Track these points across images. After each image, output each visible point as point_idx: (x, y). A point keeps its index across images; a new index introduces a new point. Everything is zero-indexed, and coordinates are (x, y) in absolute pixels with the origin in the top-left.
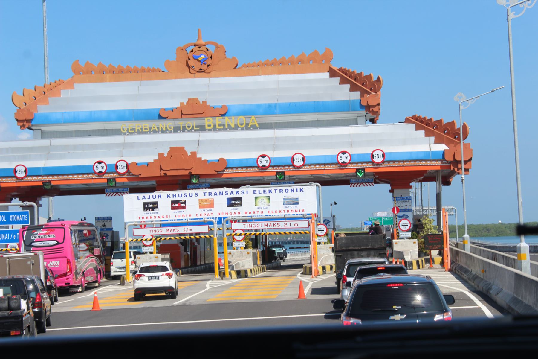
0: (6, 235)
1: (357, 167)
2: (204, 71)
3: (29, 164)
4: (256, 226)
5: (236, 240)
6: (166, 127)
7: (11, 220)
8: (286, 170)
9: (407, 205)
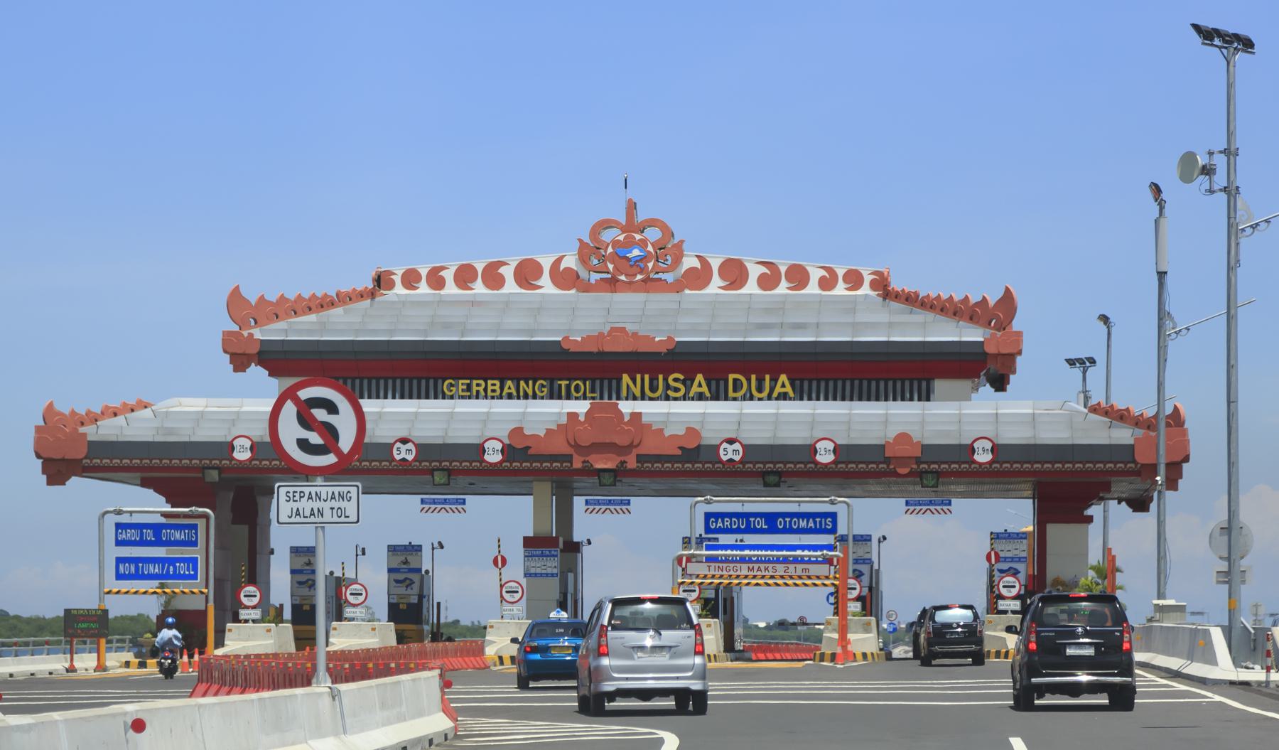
0: (157, 565)
7: (164, 539)
9: (1017, 549)
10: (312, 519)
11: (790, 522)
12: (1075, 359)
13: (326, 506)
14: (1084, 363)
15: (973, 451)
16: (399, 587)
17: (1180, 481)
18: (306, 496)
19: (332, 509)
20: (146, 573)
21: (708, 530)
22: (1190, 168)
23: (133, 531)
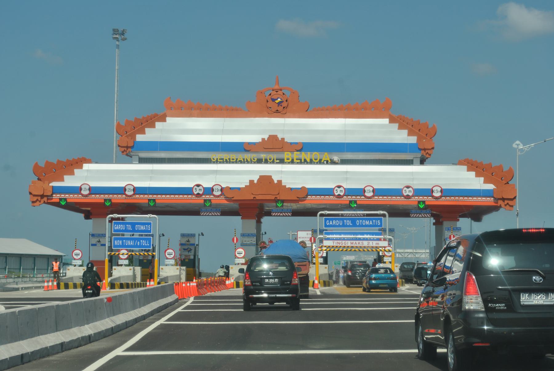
0: (132, 241)
1: (419, 200)
2: (280, 112)
3: (137, 184)
4: (344, 243)
5: (237, 257)
6: (251, 159)
7: (136, 229)
8: (358, 199)
11: (362, 222)
15: (364, 191)
16: (185, 252)
20: (127, 245)
21: (326, 226)
23: (122, 225)
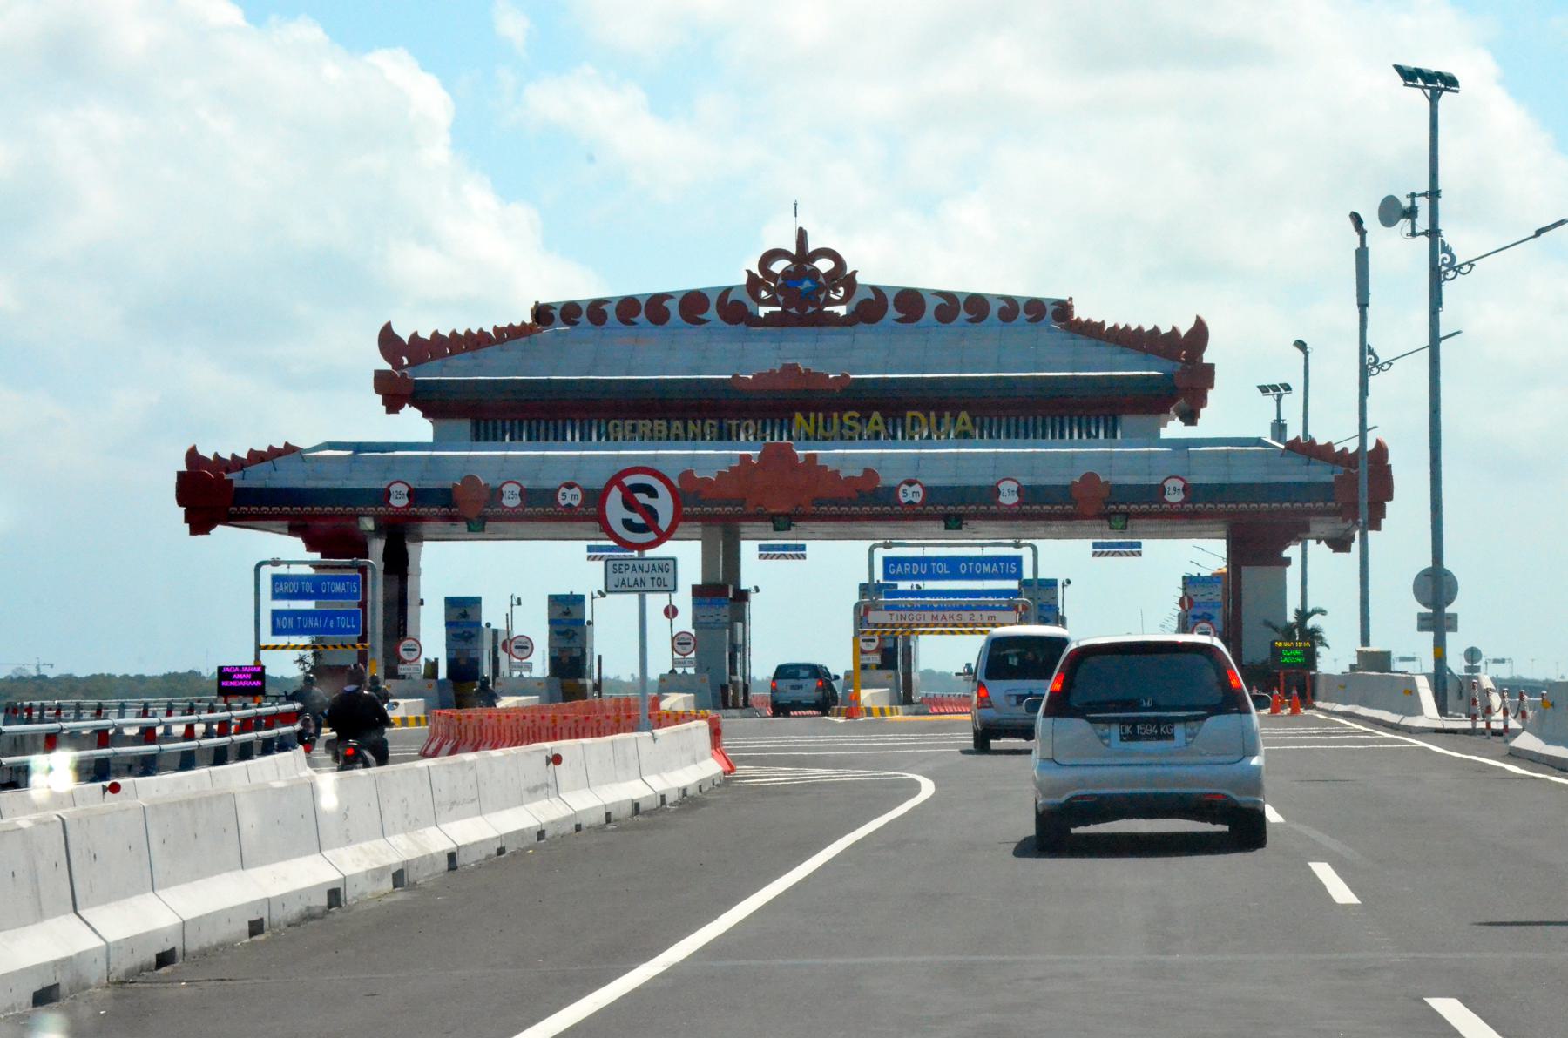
7: (324, 591)
10: (636, 588)
12: (1269, 386)
13: (648, 576)
14: (1279, 390)
17: (1383, 520)
18: (630, 570)
19: (653, 579)
21: (887, 576)
22: (1392, 211)
